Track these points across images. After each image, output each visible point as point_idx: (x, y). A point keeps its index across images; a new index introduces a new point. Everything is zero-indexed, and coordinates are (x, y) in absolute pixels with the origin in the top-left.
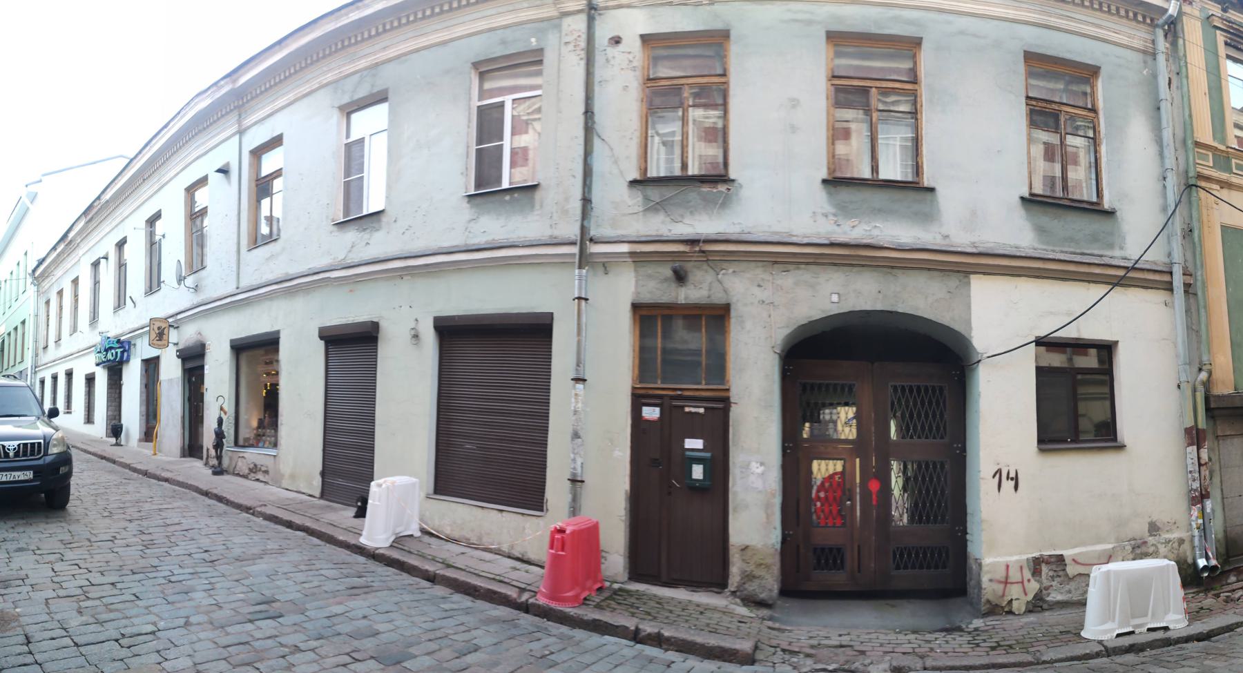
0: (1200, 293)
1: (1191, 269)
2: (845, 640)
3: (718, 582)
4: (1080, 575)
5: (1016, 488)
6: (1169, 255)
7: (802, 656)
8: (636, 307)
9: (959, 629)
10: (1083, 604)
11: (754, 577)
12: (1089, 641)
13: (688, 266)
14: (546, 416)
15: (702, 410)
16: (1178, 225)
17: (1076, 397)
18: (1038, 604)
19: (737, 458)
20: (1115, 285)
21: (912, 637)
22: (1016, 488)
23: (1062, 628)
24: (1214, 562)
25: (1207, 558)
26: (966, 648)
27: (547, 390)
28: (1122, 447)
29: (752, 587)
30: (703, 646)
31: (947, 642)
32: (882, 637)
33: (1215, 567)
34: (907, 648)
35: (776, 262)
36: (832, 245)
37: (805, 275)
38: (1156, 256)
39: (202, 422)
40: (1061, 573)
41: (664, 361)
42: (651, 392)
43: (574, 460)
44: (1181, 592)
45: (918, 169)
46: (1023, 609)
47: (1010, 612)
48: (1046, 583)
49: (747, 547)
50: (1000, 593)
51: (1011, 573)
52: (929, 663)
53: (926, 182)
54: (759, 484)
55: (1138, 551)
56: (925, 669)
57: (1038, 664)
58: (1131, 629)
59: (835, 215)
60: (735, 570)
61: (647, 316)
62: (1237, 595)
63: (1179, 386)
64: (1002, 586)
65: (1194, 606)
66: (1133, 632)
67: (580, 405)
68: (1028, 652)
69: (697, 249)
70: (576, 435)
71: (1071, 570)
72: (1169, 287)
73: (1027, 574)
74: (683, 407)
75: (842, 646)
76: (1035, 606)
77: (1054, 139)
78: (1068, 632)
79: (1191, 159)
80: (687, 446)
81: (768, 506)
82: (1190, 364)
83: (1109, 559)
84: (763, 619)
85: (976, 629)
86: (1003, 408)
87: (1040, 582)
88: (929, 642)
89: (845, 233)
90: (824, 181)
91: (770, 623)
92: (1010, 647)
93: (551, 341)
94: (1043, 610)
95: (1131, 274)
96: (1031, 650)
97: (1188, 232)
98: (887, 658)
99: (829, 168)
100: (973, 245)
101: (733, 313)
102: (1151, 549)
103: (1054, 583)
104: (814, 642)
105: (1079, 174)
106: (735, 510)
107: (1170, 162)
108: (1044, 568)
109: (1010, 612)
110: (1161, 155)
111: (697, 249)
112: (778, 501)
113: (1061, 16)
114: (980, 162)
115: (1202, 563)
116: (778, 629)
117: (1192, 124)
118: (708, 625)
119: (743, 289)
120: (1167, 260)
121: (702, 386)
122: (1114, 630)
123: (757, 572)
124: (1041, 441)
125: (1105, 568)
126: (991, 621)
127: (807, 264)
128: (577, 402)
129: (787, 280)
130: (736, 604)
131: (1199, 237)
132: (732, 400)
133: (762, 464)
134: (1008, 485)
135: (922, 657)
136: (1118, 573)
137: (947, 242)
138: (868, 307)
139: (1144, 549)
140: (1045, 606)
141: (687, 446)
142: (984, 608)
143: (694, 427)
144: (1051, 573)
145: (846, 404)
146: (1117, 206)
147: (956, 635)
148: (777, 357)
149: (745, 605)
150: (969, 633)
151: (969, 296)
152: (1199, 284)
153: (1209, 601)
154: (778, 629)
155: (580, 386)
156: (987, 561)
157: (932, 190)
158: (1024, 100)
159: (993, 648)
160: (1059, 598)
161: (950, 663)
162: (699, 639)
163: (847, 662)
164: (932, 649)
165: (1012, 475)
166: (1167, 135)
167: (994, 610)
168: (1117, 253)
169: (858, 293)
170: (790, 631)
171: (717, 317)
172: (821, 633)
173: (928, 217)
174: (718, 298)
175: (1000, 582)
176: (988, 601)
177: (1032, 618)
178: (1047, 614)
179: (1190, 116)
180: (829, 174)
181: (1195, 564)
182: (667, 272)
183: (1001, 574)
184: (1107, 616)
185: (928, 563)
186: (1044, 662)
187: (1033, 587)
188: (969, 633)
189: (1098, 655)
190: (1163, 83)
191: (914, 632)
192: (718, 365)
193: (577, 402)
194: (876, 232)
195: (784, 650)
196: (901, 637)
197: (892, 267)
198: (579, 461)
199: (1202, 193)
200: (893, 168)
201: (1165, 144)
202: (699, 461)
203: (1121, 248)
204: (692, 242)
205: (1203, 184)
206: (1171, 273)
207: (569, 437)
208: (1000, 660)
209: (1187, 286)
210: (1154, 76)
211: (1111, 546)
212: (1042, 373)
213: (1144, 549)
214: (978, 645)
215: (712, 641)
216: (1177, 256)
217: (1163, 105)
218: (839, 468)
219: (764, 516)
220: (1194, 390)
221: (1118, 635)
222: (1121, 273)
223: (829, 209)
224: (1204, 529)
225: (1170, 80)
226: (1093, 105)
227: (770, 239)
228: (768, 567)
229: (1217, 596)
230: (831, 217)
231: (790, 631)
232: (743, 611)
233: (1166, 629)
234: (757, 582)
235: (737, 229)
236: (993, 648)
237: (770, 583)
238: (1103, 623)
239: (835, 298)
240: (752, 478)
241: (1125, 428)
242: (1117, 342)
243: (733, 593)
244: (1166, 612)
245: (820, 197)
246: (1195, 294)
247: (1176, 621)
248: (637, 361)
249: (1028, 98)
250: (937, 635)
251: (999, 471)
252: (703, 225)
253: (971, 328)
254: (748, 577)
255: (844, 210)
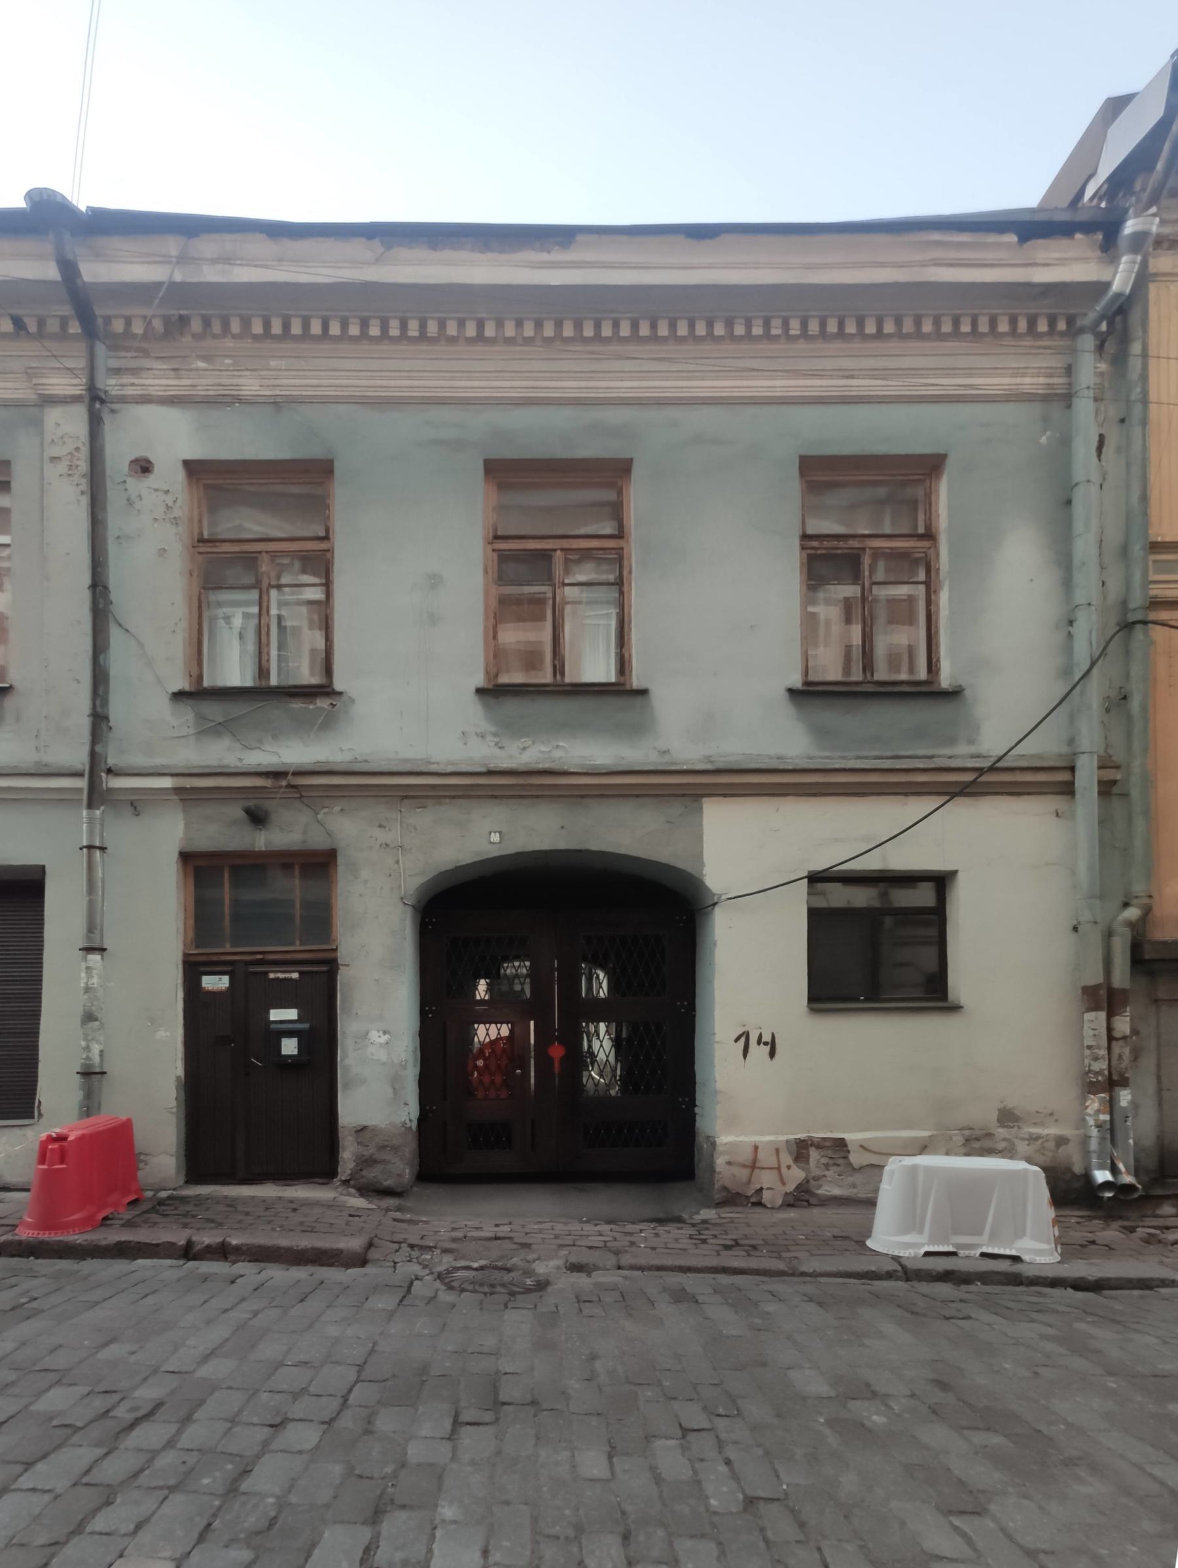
0: (1135, 794)
1: (1118, 756)
2: (504, 1230)
3: (322, 1167)
4: (872, 1165)
5: (772, 1054)
6: (1071, 742)
7: (437, 1252)
8: (186, 857)
9: (679, 1220)
10: (871, 1203)
11: (376, 1162)
12: (876, 1253)
13: (269, 805)
14: (37, 997)
15: (295, 976)
16: (1095, 692)
17: (878, 947)
18: (801, 1197)
19: (348, 1029)
20: (953, 795)
21: (605, 1228)
22: (772, 1054)
23: (837, 1232)
24: (1128, 1179)
25: (1114, 1170)
26: (685, 1243)
27: (38, 963)
28: (956, 1008)
29: (371, 1174)
30: (289, 1250)
31: (657, 1235)
32: (559, 1228)
33: (1129, 1188)
34: (596, 1241)
35: (406, 797)
36: (490, 773)
37: (451, 811)
38: (1045, 746)
39: (684, 871)
40: (840, 1161)
41: (236, 918)
42: (215, 958)
43: (87, 1049)
44: (1051, 1213)
45: (623, 665)
46: (779, 1202)
47: (759, 1204)
48: (815, 1171)
49: (364, 1128)
50: (745, 1180)
51: (761, 1155)
52: (626, 1260)
53: (636, 683)
54: (382, 1056)
55: (976, 1145)
56: (619, 1268)
57: (793, 1275)
58: (951, 1249)
59: (495, 735)
60: (348, 1155)
61: (199, 866)
62: (1172, 1236)
63: (1075, 929)
64: (745, 1172)
65: (1079, 1235)
66: (954, 1254)
67: (95, 980)
68: (779, 1257)
69: (284, 783)
70: (89, 1017)
71: (856, 1158)
72: (1068, 790)
73: (786, 1159)
74: (266, 973)
75: (496, 1238)
76: (797, 1199)
77: (850, 591)
78: (845, 1238)
79: (1137, 577)
80: (272, 1018)
81: (395, 1081)
82: (1102, 897)
83: (923, 1148)
84: (388, 1210)
85: (704, 1222)
86: (751, 967)
87: (807, 1171)
88: (631, 1234)
89: (511, 757)
90: (480, 691)
91: (398, 1215)
92: (754, 1247)
93: (43, 907)
94: (810, 1205)
95: (983, 779)
96: (784, 1255)
97: (1119, 701)
98: (564, 1252)
99: (487, 673)
100: (708, 759)
101: (340, 860)
102: (1001, 1145)
103: (827, 1173)
104: (459, 1234)
105: (893, 639)
106: (346, 1086)
107: (1087, 588)
108: (814, 1154)
109: (759, 1204)
110: (1068, 584)
111: (284, 783)
112: (411, 1074)
113: (872, 374)
114: (717, 633)
115: (1102, 1176)
116: (409, 1222)
117: (1145, 514)
118: (301, 1223)
119: (347, 827)
120: (1065, 750)
121: (297, 947)
122: (922, 1245)
123: (379, 1156)
124: (811, 999)
125: (909, 1161)
126: (727, 1213)
127: (454, 797)
128: (90, 976)
129: (423, 818)
130: (349, 1195)
131: (1144, 708)
132: (339, 961)
133: (385, 1033)
134: (759, 1052)
135: (616, 1253)
136: (930, 1171)
137: (666, 758)
138: (546, 845)
139: (987, 1143)
140: (813, 1201)
141: (272, 1018)
142: (718, 1197)
143: (284, 995)
144: (824, 1160)
145: (517, 958)
146: (963, 681)
147: (672, 1228)
148: (409, 910)
149: (362, 1195)
150: (694, 1225)
151: (701, 825)
152: (1135, 780)
153: (1111, 1234)
154: (409, 1222)
155: (95, 958)
156: (724, 1139)
157: (643, 692)
158: (796, 542)
159: (727, 1247)
160: (836, 1192)
161: (657, 1262)
162: (284, 1242)
163: (502, 1257)
164: (632, 1244)
165: (767, 1038)
166: (1084, 547)
167: (732, 1199)
168: (962, 749)
169: (537, 831)
170: (426, 1222)
171: (320, 864)
172: (470, 1223)
173: (638, 729)
174: (318, 841)
175: (745, 1166)
176: (725, 1188)
177: (792, 1214)
178: (815, 1211)
179: (1144, 498)
180: (489, 680)
181: (1087, 1177)
182: (236, 811)
183: (746, 1156)
184: (911, 1222)
185: (643, 1137)
186: (803, 1274)
187: (796, 1175)
188: (694, 1225)
189: (889, 1275)
190: (1083, 449)
191: (609, 1222)
192: (320, 919)
193: (90, 976)
194: (558, 754)
195: (412, 1246)
196: (589, 1228)
197: (582, 796)
198: (96, 1049)
199: (1158, 633)
200: (596, 668)
201: (1077, 561)
202: (290, 1034)
203: (971, 742)
204: (277, 775)
205: (1164, 615)
206: (1072, 769)
207: (77, 1021)
208: (736, 1264)
209: (1106, 789)
210: (1065, 442)
211: (927, 1134)
212: (816, 916)
213: (987, 1143)
214: (704, 1241)
215: (304, 1242)
216: (1090, 737)
217: (1078, 496)
218: (505, 1031)
219: (390, 1091)
220: (1109, 934)
221: (927, 1254)
222: (969, 777)
223: (486, 726)
224: (1111, 1131)
225: (1101, 437)
226: (928, 527)
227: (395, 769)
228: (395, 1149)
229: (1132, 1230)
230: (489, 738)
231: (426, 1222)
232: (359, 1202)
233: (1016, 1259)
234: (379, 1167)
235: (347, 757)
236: (727, 1247)
237: (400, 1167)
238: (905, 1231)
239: (495, 838)
240: (371, 1049)
241: (959, 983)
242: (954, 873)
243: (346, 1183)
244: (1020, 1233)
245: (474, 713)
246: (1125, 795)
247: (1036, 1245)
248: (191, 922)
249: (805, 537)
250: (642, 1226)
251: (746, 1035)
252: (294, 753)
253: (702, 864)
254: (365, 1162)
255: (509, 729)
